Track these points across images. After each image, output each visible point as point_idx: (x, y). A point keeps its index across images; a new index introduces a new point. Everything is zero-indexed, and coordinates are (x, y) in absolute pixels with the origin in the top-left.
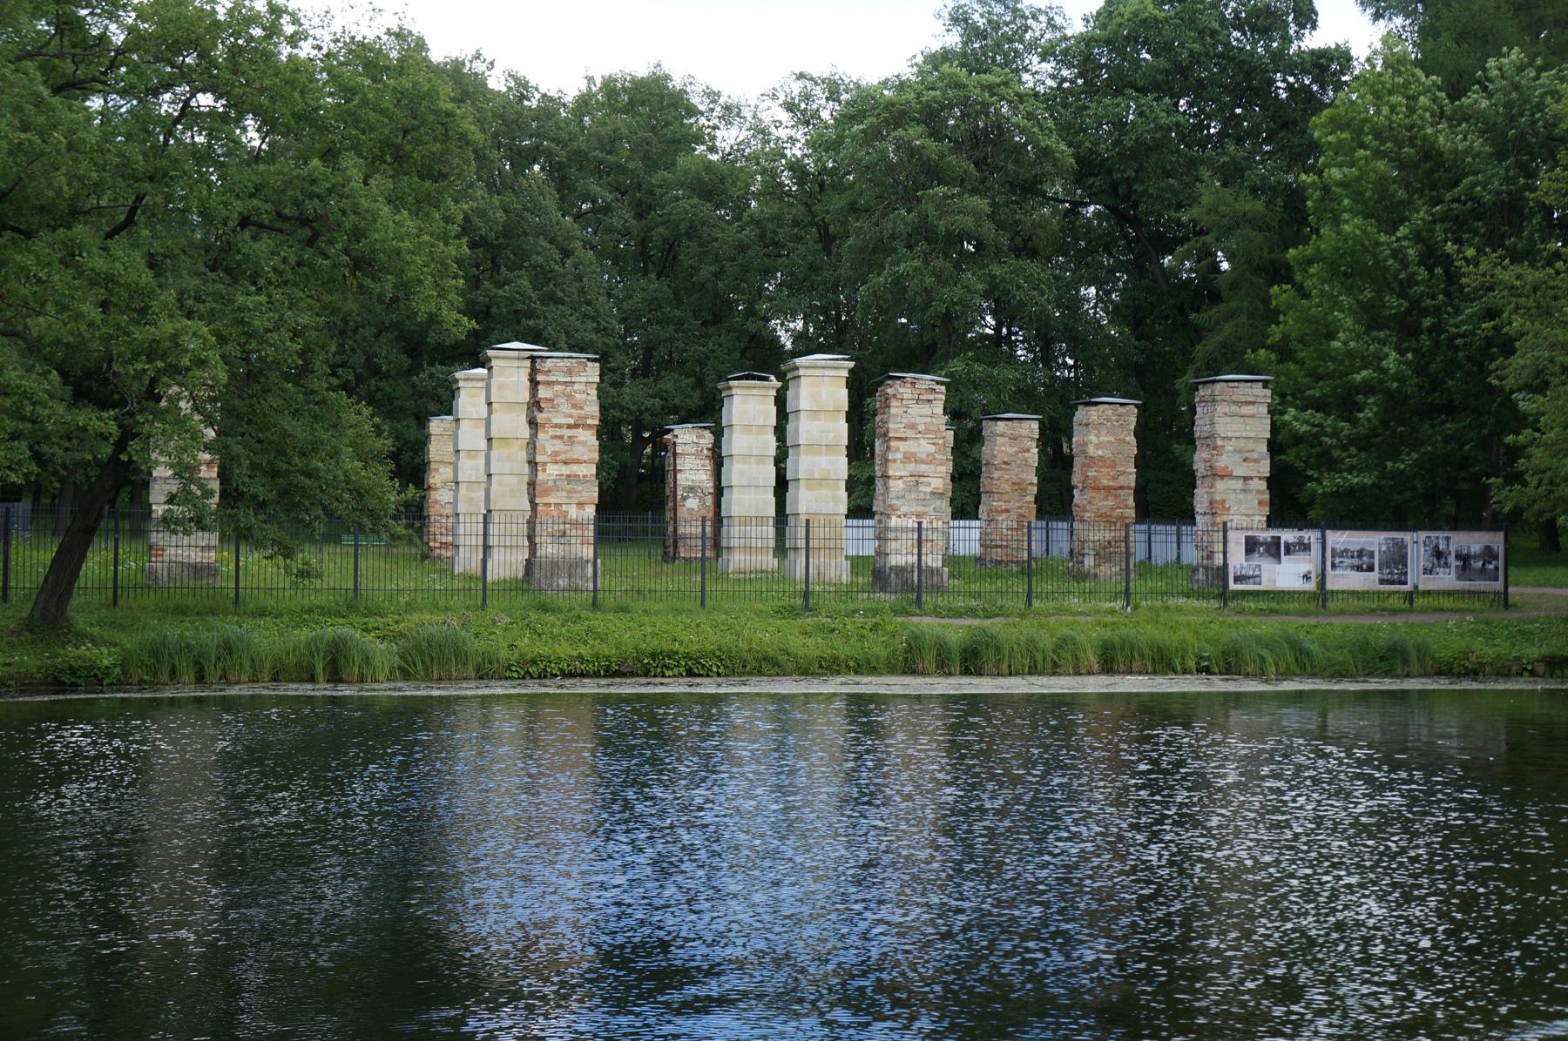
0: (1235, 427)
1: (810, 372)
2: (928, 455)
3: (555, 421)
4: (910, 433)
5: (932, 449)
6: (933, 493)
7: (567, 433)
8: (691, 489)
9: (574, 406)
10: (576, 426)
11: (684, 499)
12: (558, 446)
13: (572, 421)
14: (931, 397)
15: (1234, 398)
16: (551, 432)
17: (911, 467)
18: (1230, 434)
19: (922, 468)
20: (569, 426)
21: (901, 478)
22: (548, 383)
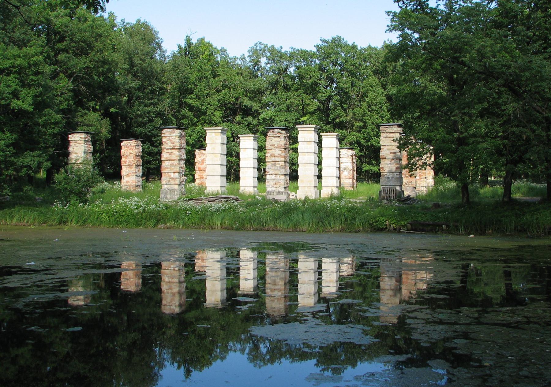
0: (386, 141)
2: (278, 154)
3: (167, 148)
4: (272, 147)
5: (280, 152)
7: (170, 151)
8: (345, 169)
9: (172, 143)
10: (172, 149)
11: (343, 172)
12: (168, 155)
13: (171, 148)
14: (279, 135)
15: (386, 131)
16: (166, 151)
18: (385, 144)
19: (277, 159)
20: (171, 149)
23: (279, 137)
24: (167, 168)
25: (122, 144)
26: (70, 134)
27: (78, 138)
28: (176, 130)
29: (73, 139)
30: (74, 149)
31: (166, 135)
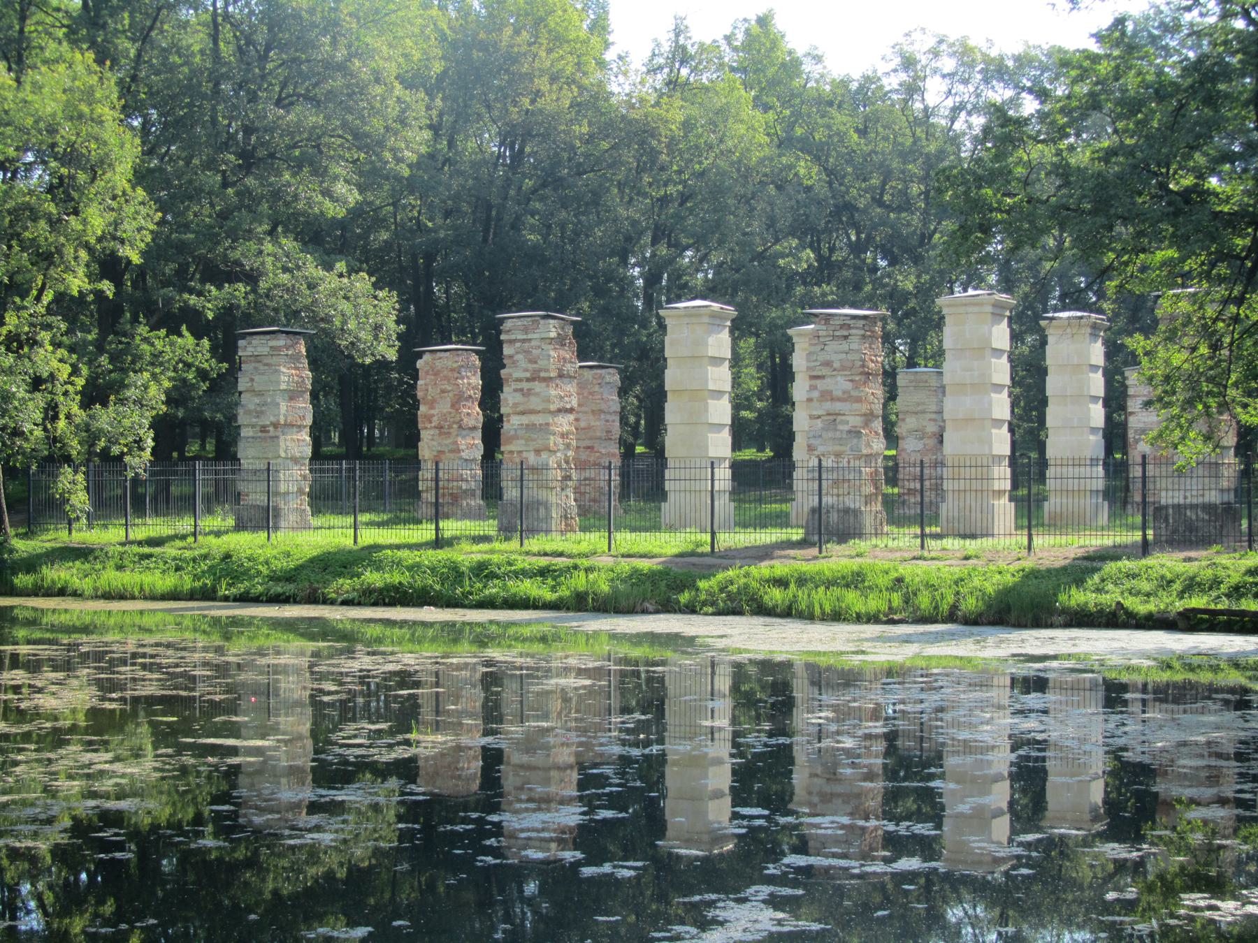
1: (952, 310)
2: (844, 392)
5: (849, 386)
6: (849, 432)
7: (525, 385)
8: (1143, 431)
11: (1137, 441)
12: (518, 397)
14: (845, 333)
16: (514, 386)
17: (828, 406)
20: (528, 380)
21: (819, 417)
22: (511, 342)
23: (846, 337)
24: (516, 437)
25: (420, 364)
26: (244, 336)
27: (265, 350)
28: (542, 322)
29: (250, 351)
30: (252, 380)
31: (513, 337)
